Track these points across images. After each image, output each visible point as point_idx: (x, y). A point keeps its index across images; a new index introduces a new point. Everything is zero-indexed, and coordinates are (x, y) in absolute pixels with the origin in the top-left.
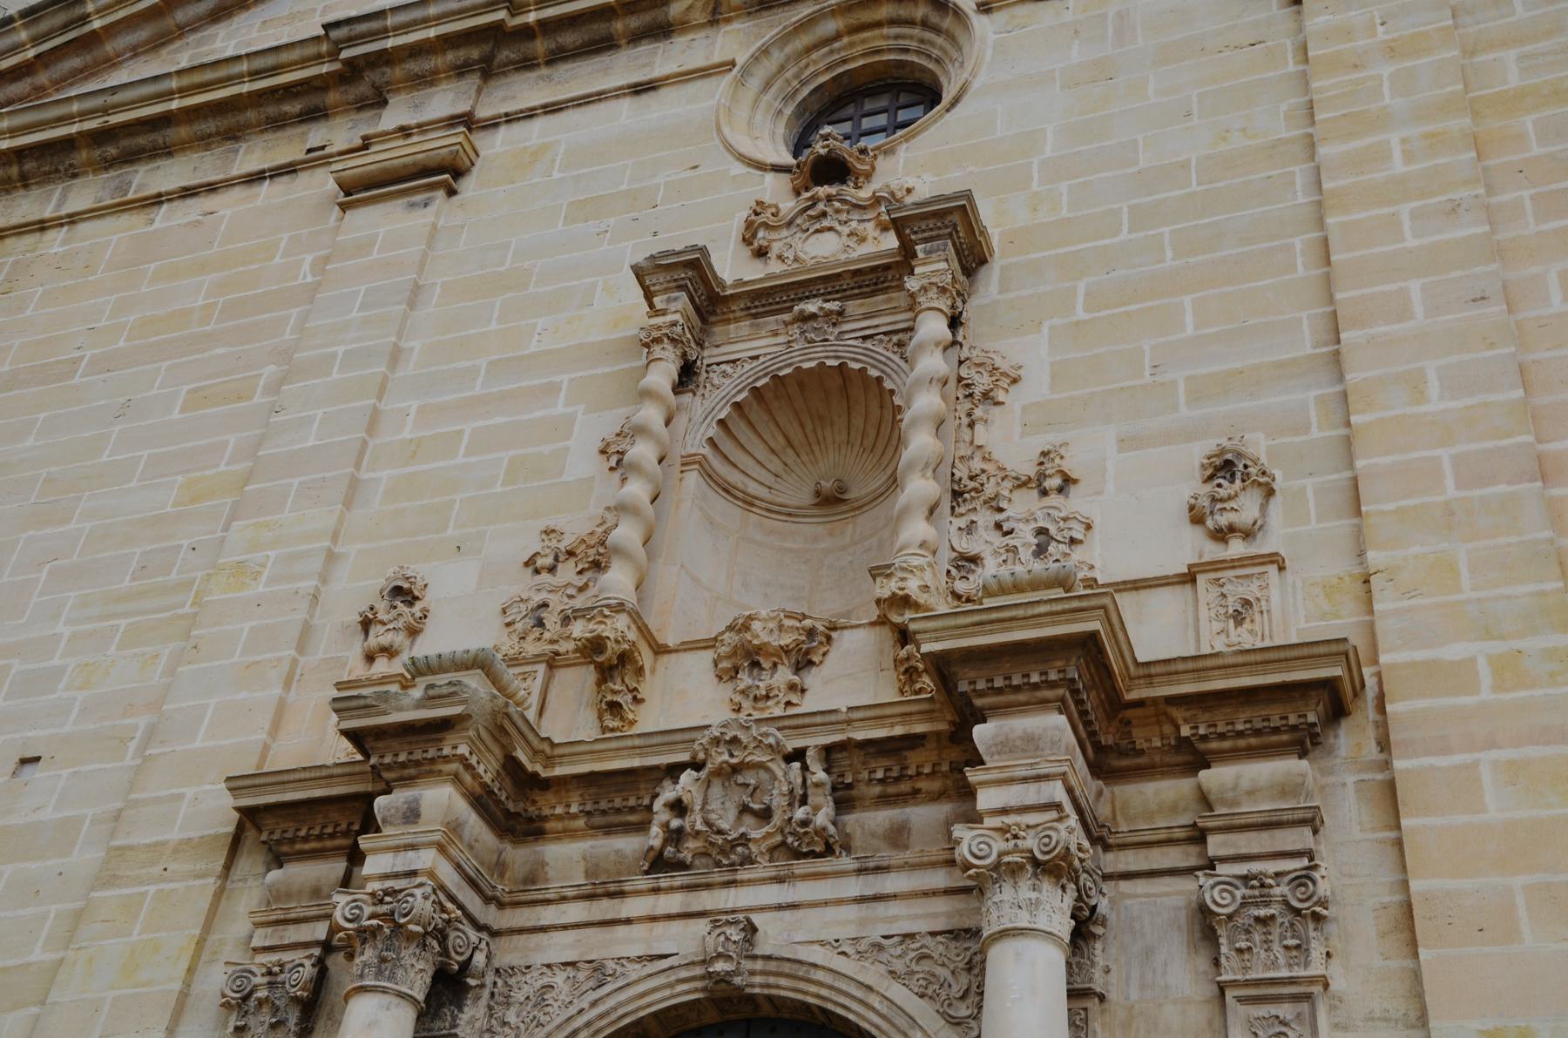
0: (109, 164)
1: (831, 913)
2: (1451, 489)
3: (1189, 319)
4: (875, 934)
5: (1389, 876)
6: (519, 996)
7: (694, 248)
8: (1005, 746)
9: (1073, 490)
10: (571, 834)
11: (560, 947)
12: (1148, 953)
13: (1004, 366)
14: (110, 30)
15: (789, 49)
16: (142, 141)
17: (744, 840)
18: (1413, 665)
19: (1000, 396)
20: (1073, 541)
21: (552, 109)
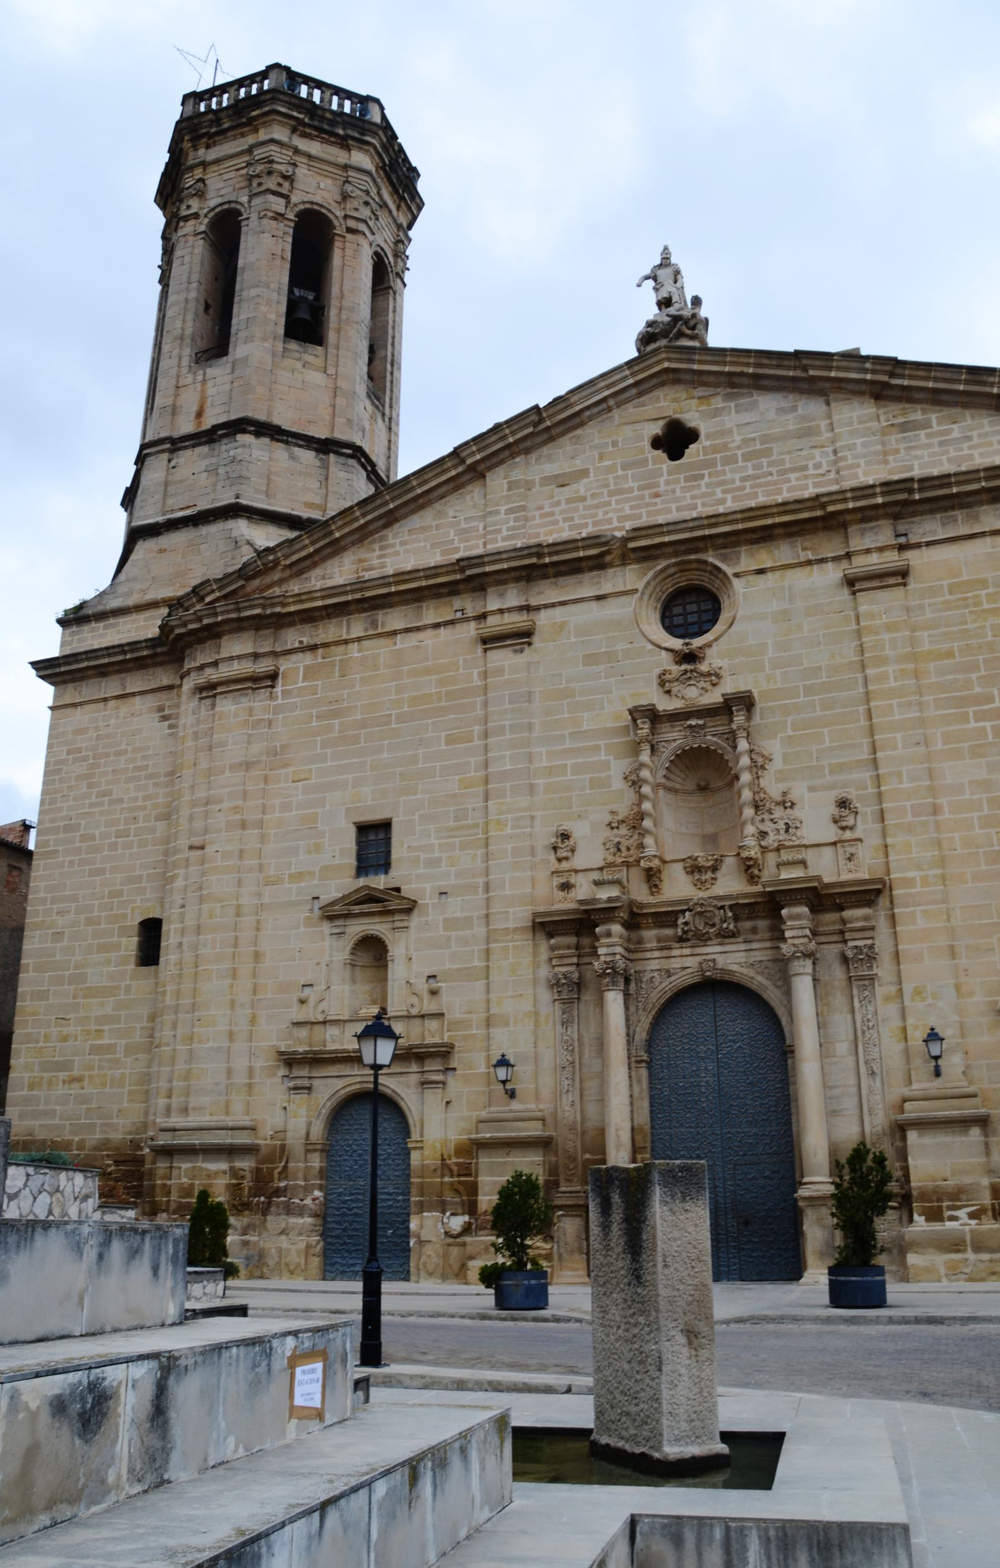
0: (364, 610)
1: (737, 954)
2: (910, 818)
3: (827, 738)
4: (752, 960)
5: (892, 943)
6: (645, 979)
7: (651, 705)
8: (792, 917)
9: (796, 807)
10: (649, 928)
11: (654, 965)
12: (830, 966)
13: (766, 753)
14: (342, 537)
15: (657, 580)
16: (379, 602)
17: (708, 933)
18: (899, 878)
19: (767, 767)
20: (797, 828)
21: (563, 603)
